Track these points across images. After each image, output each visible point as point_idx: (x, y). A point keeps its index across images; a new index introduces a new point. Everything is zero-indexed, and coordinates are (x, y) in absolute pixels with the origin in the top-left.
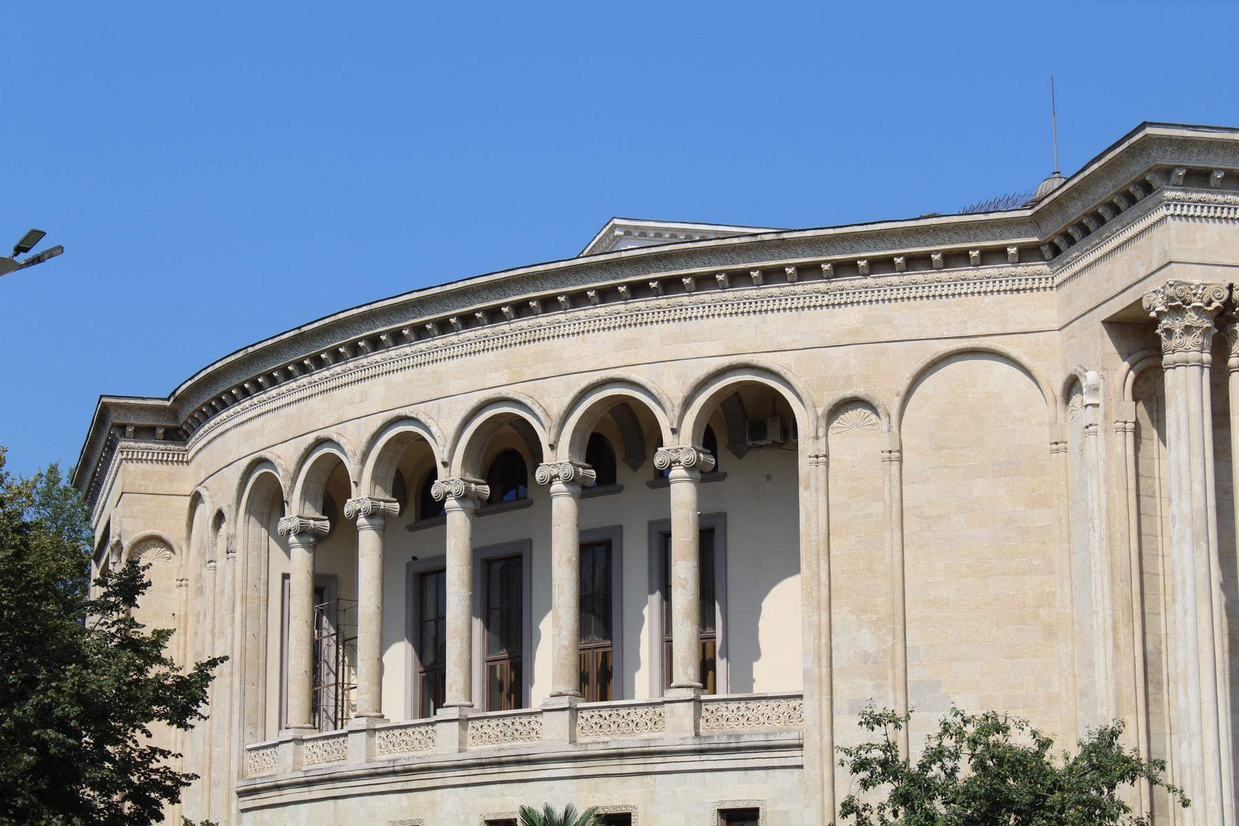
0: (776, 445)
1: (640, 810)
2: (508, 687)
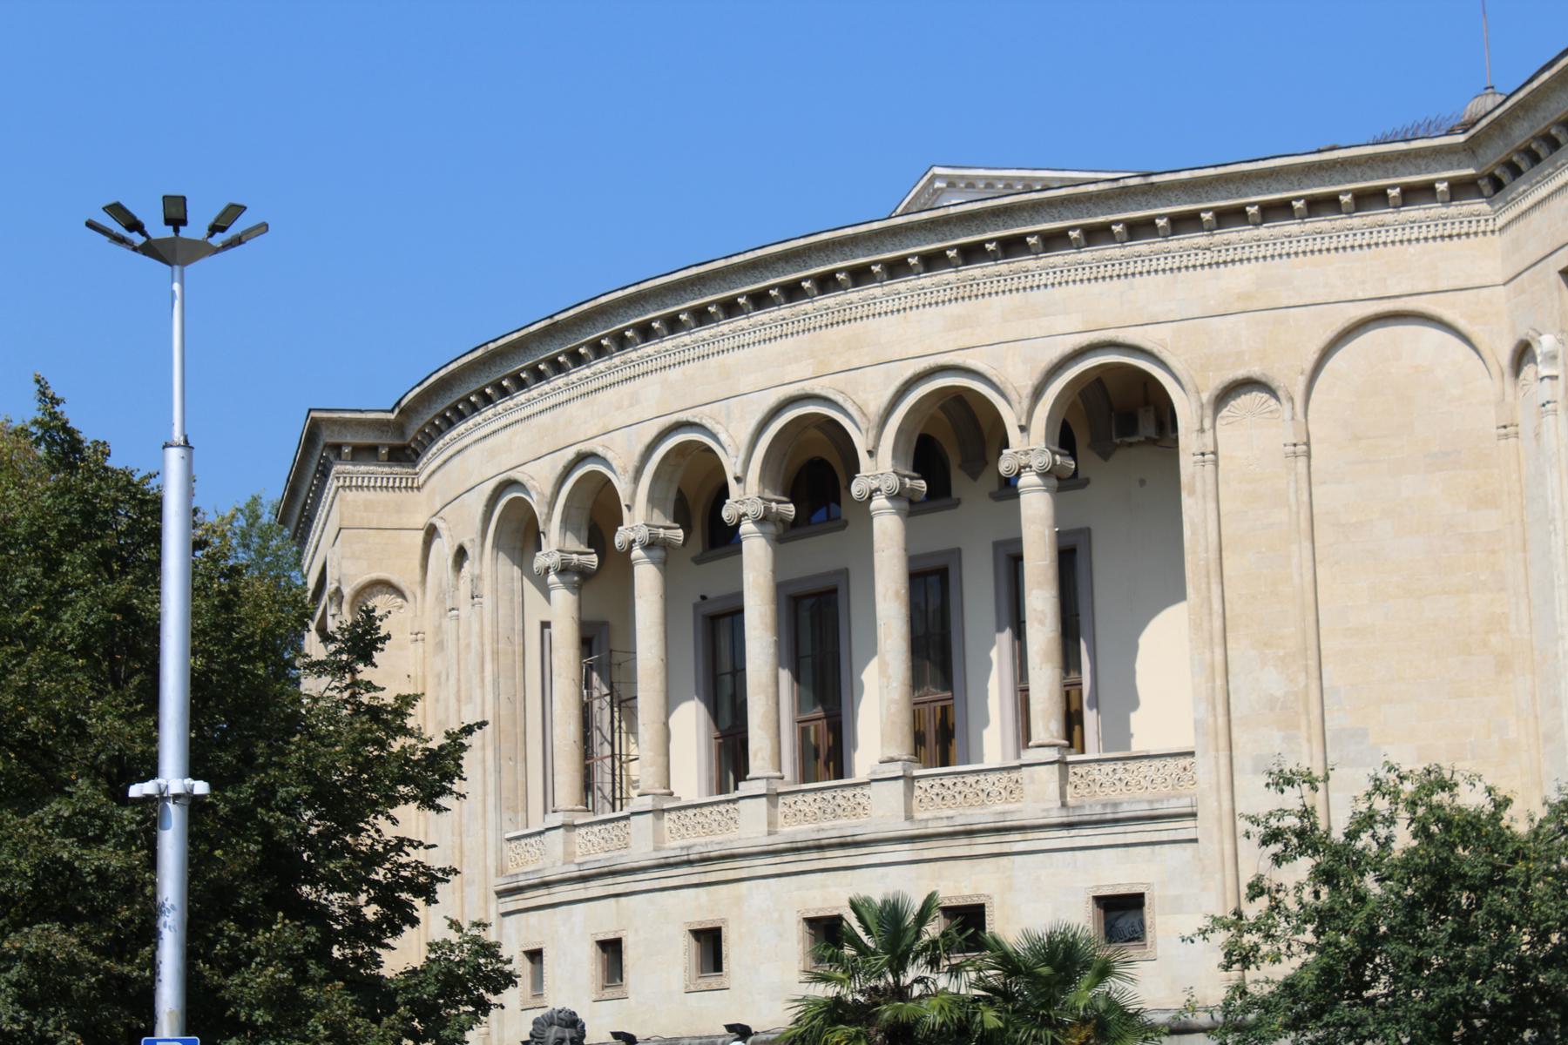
0: (1149, 441)
1: (996, 900)
2: (826, 754)
